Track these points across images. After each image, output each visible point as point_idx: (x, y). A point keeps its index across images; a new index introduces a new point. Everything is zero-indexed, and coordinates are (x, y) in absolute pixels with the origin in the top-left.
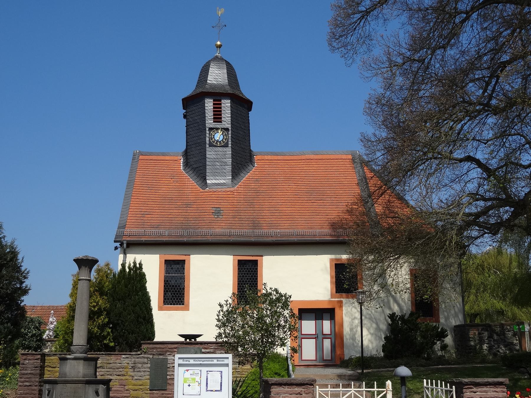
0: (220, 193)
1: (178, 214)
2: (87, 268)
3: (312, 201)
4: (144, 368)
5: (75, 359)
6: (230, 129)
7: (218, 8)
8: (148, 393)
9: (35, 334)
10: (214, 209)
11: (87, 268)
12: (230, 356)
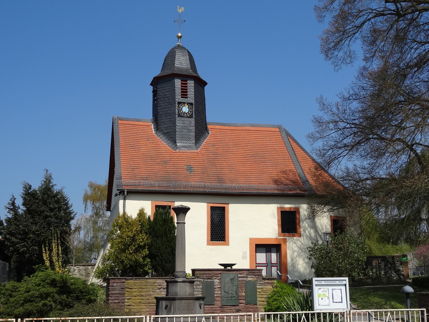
0: (188, 154)
1: (159, 169)
3: (258, 163)
7: (178, 7)
10: (186, 166)
12: (347, 279)
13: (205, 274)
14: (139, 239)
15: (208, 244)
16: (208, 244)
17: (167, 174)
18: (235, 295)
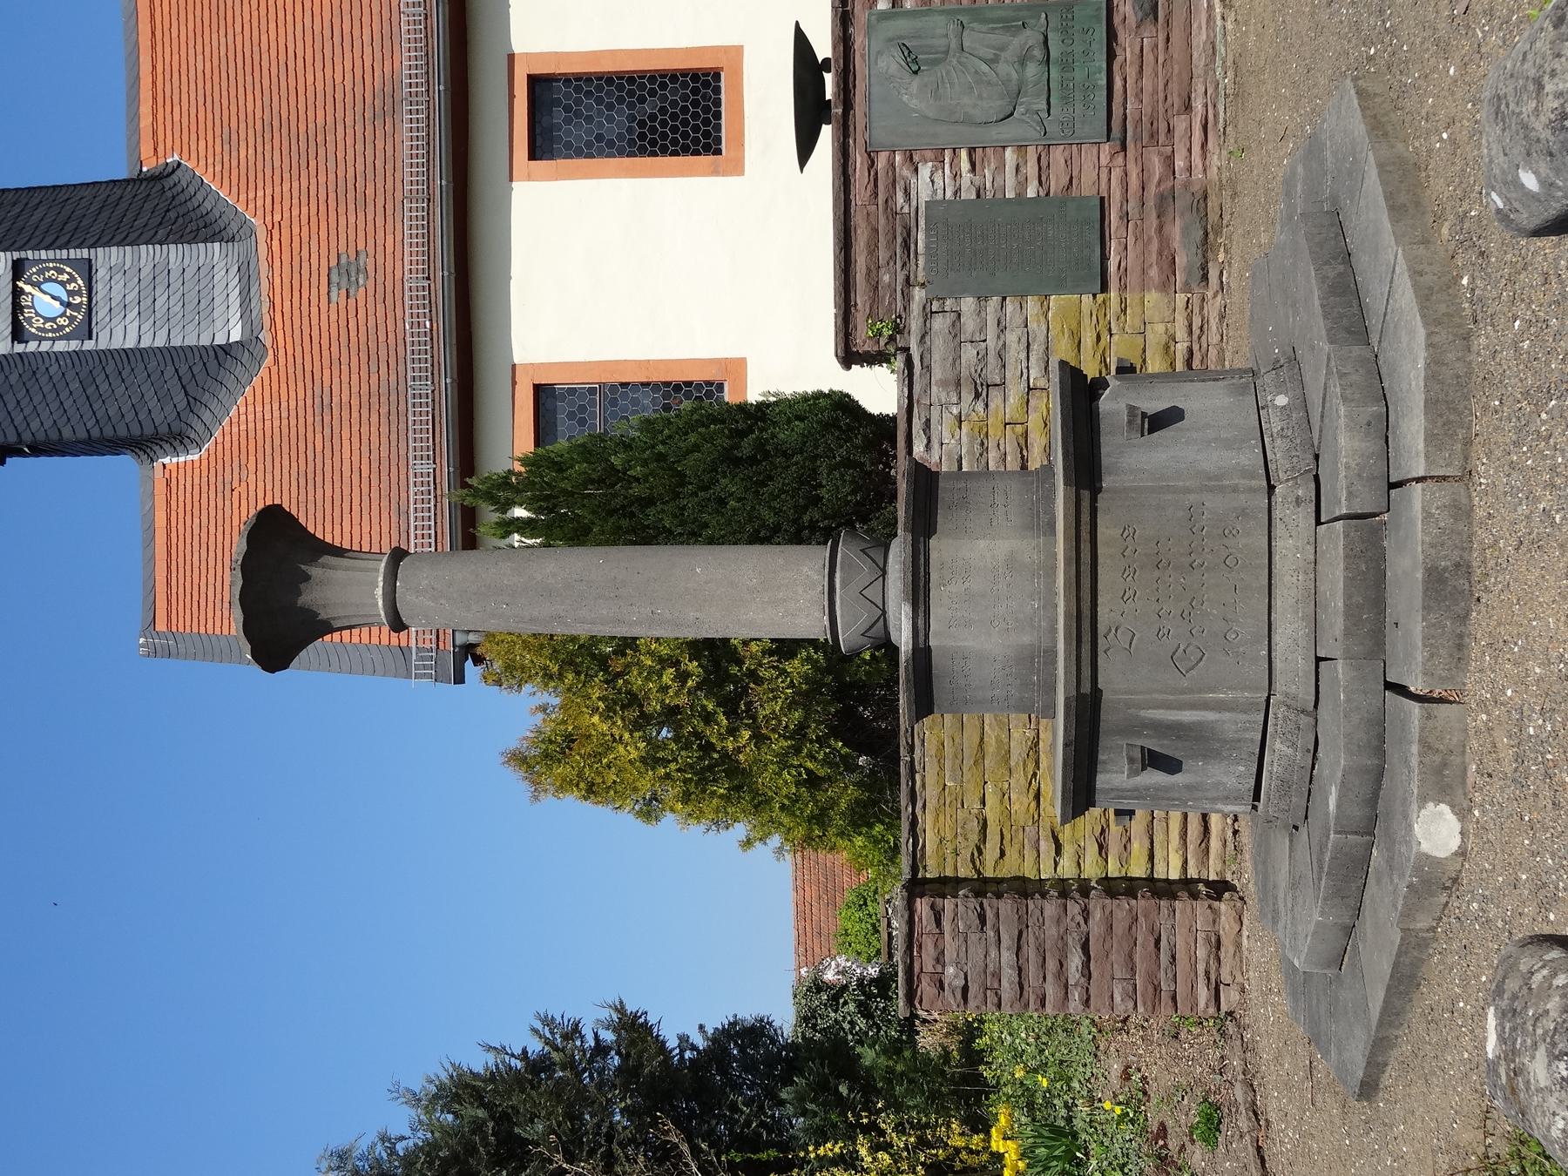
0: (277, 281)
1: (355, 440)
2: (315, 571)
4: (983, 328)
5: (919, 594)
6: (16, 255)
8: (1123, 301)
9: (860, 1004)
11: (315, 571)
13: (873, 271)
14: (664, 689)
15: (737, 168)
16: (737, 168)
17: (374, 400)
18: (1031, 37)
